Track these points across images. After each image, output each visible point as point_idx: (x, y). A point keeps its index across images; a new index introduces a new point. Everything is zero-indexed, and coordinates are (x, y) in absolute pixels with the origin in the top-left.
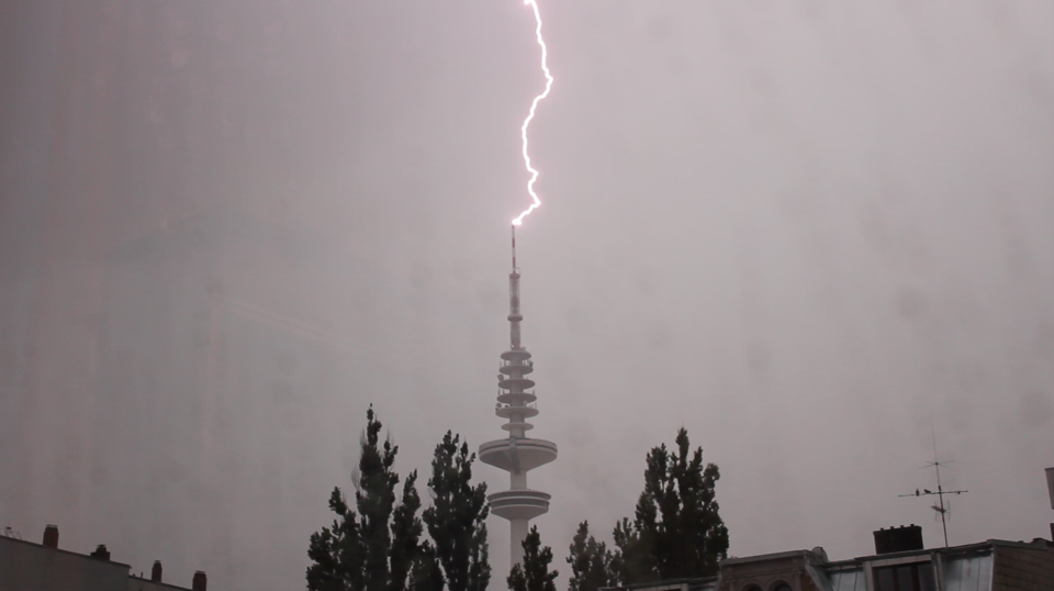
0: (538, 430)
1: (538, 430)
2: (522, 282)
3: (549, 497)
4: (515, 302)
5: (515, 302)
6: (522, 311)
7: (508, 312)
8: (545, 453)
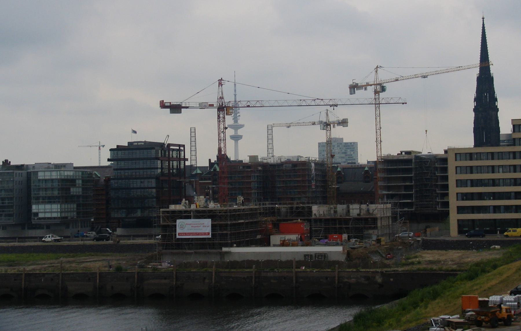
0: (240, 122)
1: (240, 122)
3: (242, 136)
4: (235, 91)
5: (235, 91)
6: (237, 93)
7: (234, 93)
8: (242, 126)
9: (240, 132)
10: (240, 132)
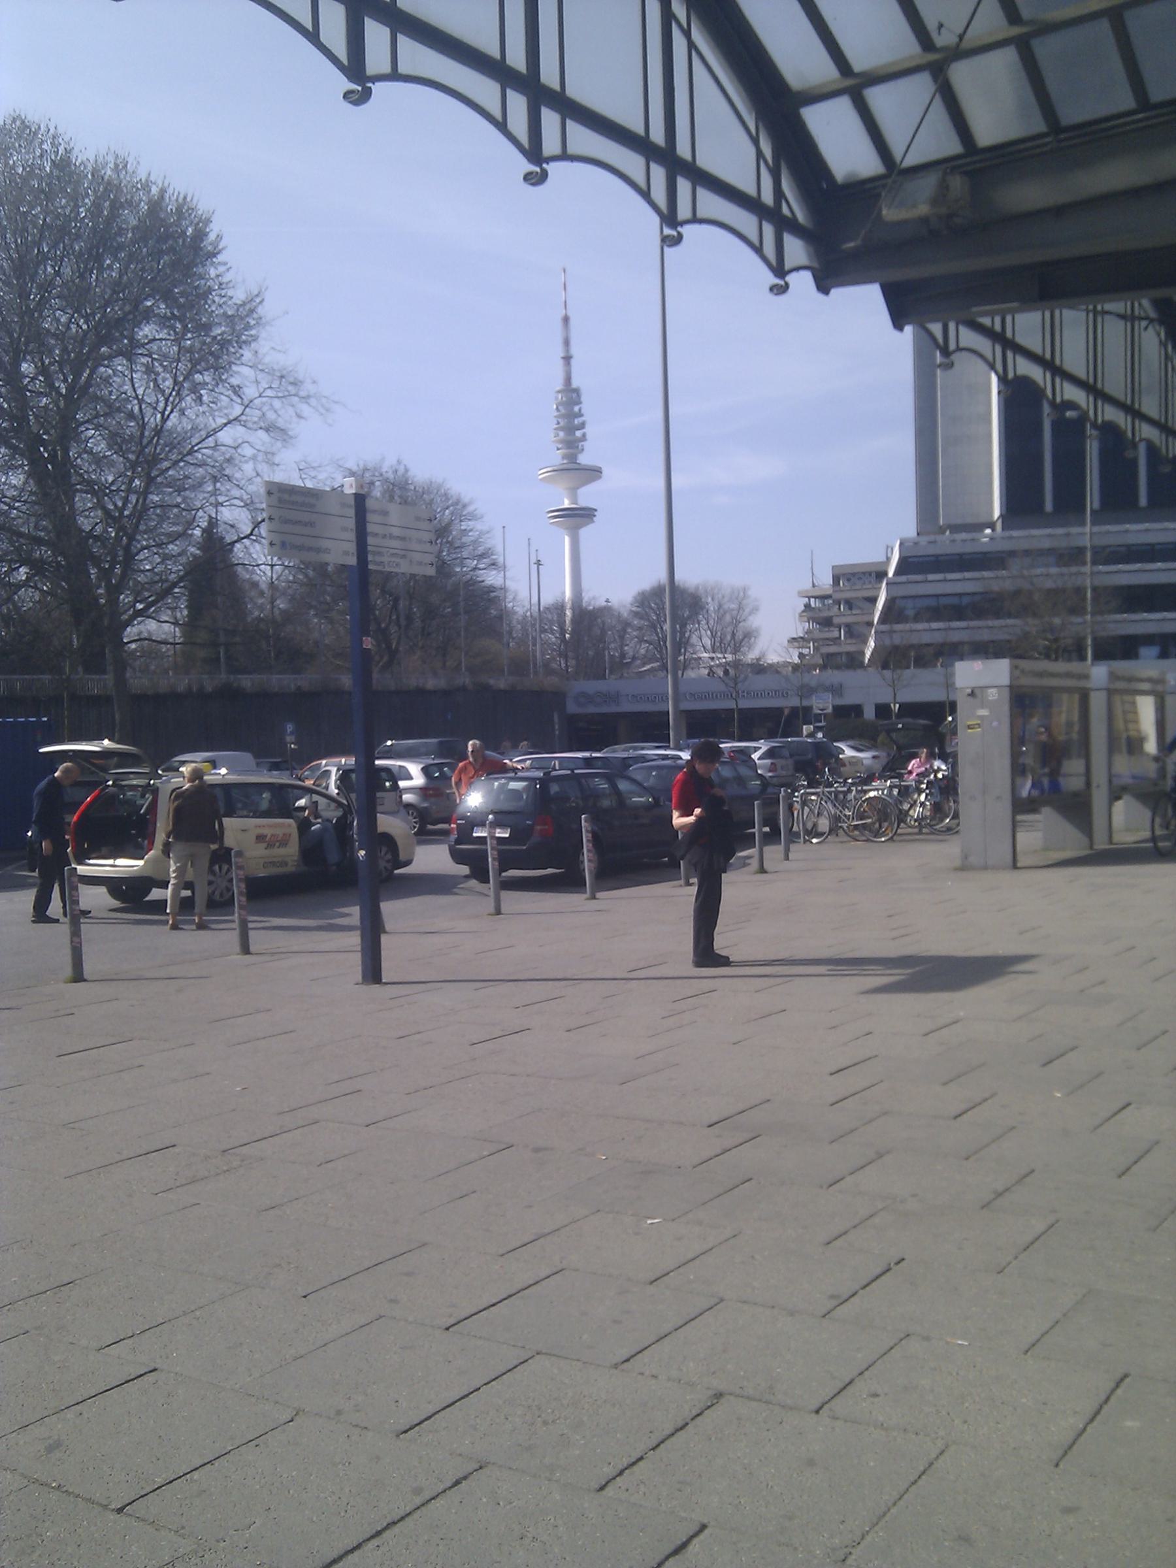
0: (584, 459)
1: (584, 459)
2: (572, 322)
4: (567, 343)
5: (567, 343)
6: (574, 350)
7: (561, 353)
8: (594, 473)
9: (588, 496)
10: (588, 496)
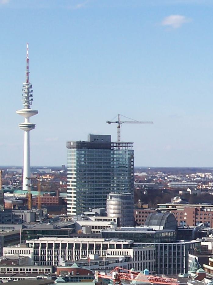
2: (30, 61)
3: (34, 125)
4: (28, 68)
